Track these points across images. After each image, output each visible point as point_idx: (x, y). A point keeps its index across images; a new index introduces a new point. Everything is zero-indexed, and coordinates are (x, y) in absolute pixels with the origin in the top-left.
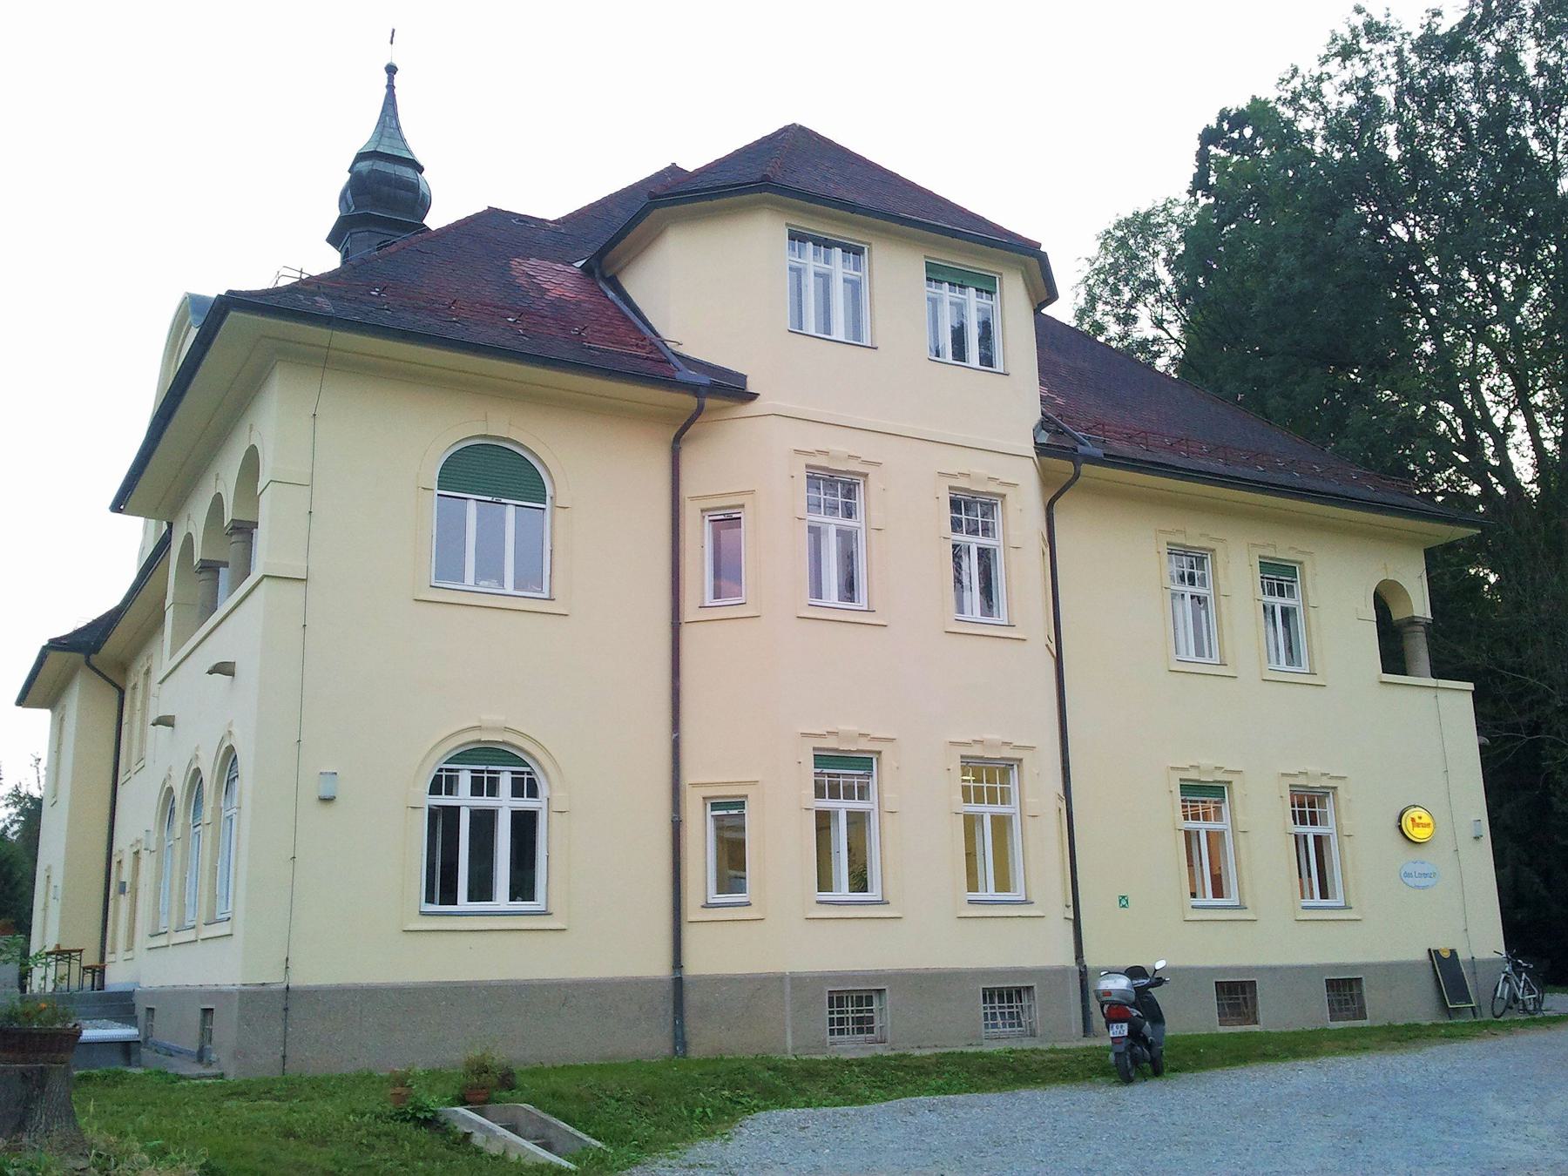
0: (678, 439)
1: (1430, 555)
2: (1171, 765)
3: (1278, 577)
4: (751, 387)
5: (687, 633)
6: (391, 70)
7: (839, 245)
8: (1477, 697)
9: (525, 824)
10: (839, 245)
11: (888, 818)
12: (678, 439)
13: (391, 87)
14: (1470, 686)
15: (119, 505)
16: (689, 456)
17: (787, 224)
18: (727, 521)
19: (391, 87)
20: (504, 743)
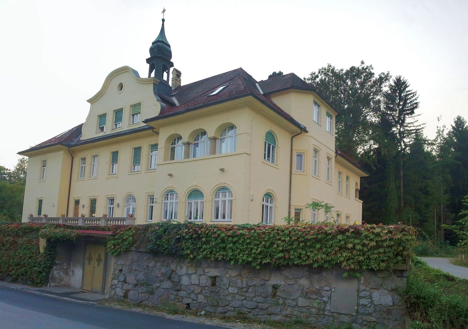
0: (293, 137)
1: (361, 178)
2: (346, 213)
3: (347, 178)
4: (307, 130)
5: (292, 175)
6: (163, 20)
7: (317, 104)
8: (363, 203)
9: (231, 202)
10: (317, 104)
11: (276, 209)
12: (293, 137)
13: (163, 25)
14: (362, 202)
15: (89, 101)
16: (294, 139)
17: (314, 99)
18: (300, 156)
19: (163, 25)
20: (270, 193)
